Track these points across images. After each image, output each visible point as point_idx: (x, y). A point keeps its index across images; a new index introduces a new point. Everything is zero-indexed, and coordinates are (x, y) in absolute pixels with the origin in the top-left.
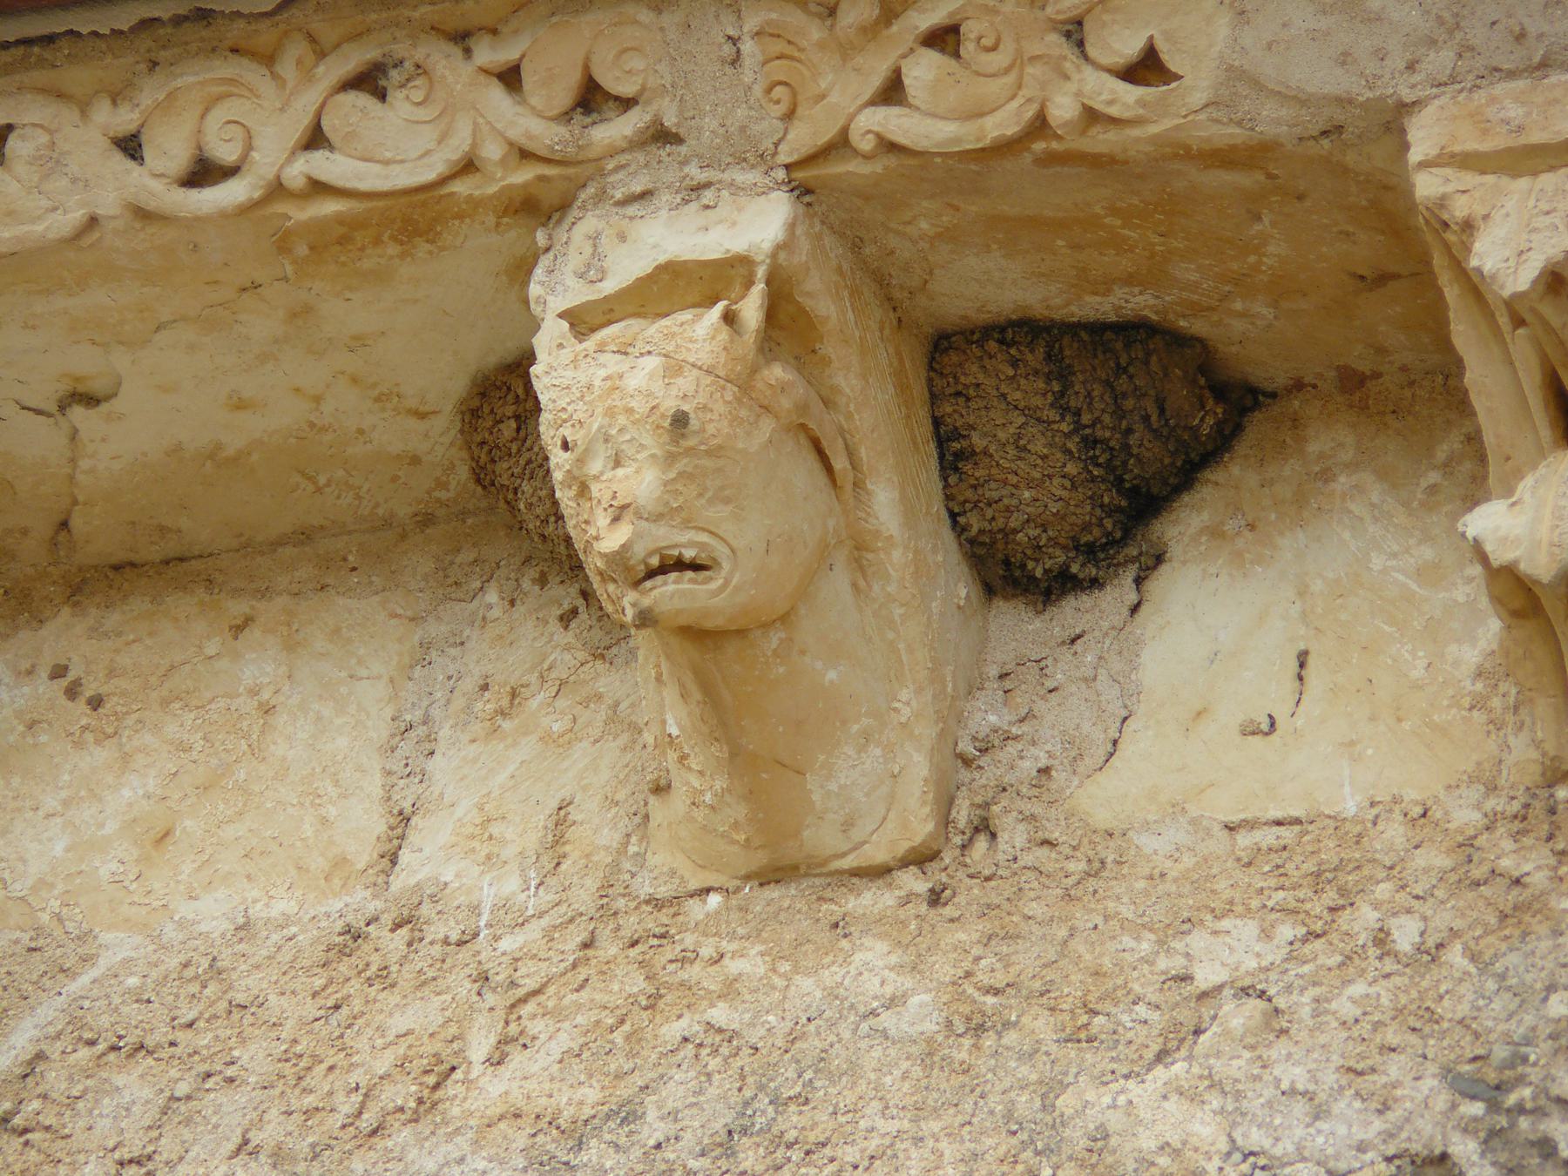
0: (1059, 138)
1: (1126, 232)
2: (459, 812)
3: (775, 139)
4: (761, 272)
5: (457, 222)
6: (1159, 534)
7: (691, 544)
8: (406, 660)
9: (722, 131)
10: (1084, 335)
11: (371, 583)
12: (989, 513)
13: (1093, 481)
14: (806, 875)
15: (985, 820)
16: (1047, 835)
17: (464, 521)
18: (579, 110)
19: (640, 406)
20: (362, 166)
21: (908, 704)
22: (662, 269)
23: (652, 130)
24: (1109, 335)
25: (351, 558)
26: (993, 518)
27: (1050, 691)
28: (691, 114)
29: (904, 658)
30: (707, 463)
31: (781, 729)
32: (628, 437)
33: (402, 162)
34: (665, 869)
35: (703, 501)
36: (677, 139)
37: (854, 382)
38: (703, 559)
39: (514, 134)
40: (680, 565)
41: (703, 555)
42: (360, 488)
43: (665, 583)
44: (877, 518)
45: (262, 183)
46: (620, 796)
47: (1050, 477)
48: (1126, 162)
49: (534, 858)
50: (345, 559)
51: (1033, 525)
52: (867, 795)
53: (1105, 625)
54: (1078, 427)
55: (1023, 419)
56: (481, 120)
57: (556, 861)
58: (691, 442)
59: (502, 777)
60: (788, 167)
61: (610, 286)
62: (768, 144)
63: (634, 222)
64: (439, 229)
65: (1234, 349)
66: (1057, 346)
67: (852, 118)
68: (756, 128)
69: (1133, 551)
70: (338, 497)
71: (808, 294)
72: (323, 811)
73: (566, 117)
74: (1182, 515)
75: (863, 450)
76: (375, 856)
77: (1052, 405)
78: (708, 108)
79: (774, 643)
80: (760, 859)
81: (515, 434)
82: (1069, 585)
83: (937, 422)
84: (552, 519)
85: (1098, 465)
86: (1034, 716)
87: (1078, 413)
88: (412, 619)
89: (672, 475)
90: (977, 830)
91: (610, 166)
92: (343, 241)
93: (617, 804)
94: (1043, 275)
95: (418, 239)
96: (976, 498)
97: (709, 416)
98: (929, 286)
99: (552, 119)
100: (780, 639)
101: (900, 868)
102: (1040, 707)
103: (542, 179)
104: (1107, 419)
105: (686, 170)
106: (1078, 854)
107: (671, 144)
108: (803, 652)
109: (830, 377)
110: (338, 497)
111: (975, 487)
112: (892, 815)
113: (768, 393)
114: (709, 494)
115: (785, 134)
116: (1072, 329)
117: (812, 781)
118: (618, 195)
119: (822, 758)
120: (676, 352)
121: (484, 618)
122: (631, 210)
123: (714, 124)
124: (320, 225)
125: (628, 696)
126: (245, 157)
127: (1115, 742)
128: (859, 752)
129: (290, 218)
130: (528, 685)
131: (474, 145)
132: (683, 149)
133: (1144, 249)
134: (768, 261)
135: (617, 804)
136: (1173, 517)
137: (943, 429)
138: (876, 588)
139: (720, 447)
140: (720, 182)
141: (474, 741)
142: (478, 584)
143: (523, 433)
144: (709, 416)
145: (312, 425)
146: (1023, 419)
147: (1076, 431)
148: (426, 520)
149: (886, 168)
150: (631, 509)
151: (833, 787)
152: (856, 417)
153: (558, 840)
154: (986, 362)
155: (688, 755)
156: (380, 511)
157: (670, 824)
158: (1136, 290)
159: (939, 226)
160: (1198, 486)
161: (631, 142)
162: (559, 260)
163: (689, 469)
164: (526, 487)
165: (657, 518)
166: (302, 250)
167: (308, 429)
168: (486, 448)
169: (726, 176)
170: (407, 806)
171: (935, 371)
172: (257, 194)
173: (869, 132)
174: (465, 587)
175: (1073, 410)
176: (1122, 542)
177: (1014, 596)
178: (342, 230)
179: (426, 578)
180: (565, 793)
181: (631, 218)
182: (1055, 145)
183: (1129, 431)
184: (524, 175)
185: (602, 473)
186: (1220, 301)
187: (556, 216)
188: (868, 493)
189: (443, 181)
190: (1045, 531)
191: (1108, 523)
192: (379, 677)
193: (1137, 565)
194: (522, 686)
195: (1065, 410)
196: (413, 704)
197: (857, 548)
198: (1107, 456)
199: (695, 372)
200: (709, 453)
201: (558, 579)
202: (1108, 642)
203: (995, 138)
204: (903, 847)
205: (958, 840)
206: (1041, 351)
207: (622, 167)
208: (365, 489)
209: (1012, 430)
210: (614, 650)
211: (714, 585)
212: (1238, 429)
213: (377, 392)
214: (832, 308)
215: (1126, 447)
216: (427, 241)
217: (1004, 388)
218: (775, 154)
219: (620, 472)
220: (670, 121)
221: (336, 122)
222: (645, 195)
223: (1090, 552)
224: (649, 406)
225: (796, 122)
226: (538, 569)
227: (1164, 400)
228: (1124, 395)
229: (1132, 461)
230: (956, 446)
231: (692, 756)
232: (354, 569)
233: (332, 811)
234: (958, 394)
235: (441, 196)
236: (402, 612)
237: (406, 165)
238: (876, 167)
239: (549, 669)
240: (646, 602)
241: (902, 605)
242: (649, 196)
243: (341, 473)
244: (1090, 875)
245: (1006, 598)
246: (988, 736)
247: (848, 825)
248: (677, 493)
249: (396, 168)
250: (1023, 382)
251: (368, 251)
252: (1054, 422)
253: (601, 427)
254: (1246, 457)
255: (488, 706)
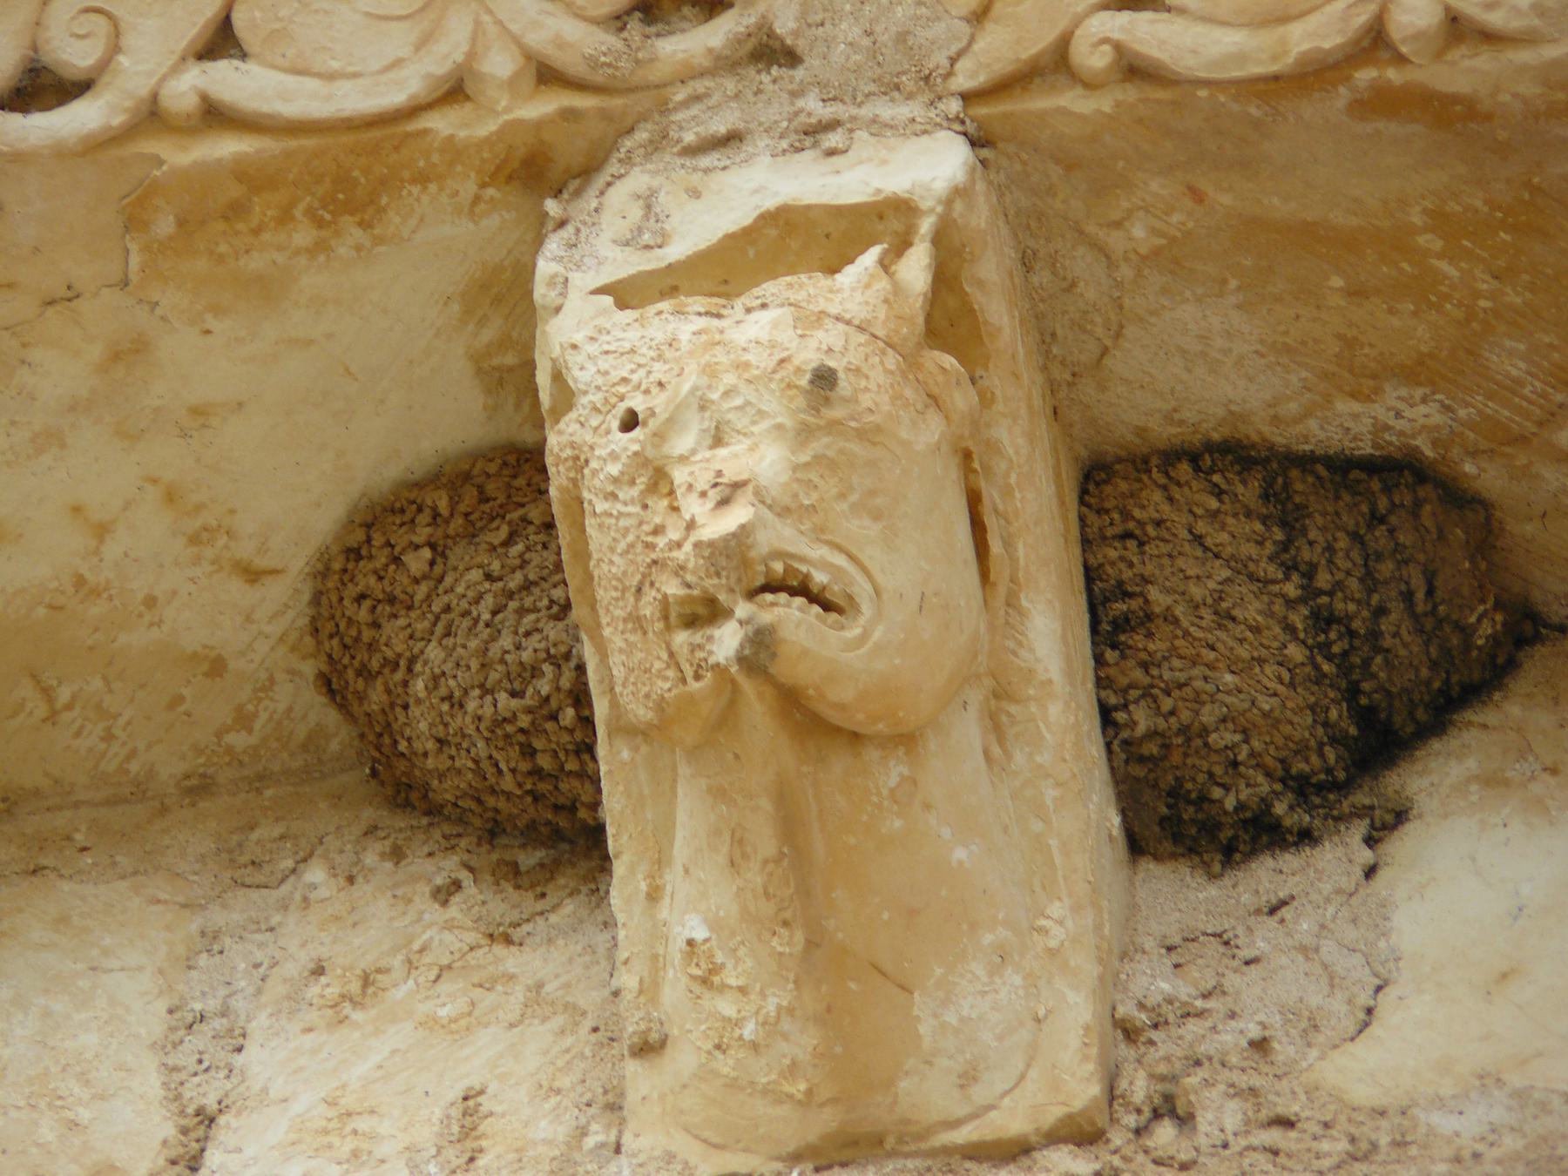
0: (1401, 60)
1: (1444, 266)
2: (297, 1108)
3: (954, 48)
4: (926, 226)
5: (416, 190)
6: (1397, 787)
7: (825, 565)
8: (181, 950)
9: (866, 42)
10: (1321, 470)
11: (114, 864)
12: (1167, 704)
13: (1317, 683)
14: (893, 1154)
15: (1168, 1098)
16: (1280, 1110)
17: (259, 791)
18: (638, 15)
19: (761, 360)
20: (291, 81)
21: (1061, 923)
22: (768, 218)
23: (750, 45)
24: (1355, 474)
25: (78, 837)
26: (1172, 713)
27: (1247, 963)
28: (818, 18)
29: (1058, 860)
30: (854, 447)
31: (886, 916)
32: (739, 401)
33: (355, 75)
34: (656, 1153)
35: (845, 506)
36: (791, 58)
37: (1020, 441)
38: (835, 594)
39: (537, 40)
40: (803, 590)
41: (836, 588)
42: (116, 716)
43: (788, 606)
44: (1032, 650)
45: (128, 104)
46: (565, 1082)
47: (1261, 661)
48: (1488, 117)
49: (433, 1151)
50: (69, 838)
51: (1231, 726)
52: (1000, 1038)
53: (1327, 888)
54: (1310, 592)
55: (1226, 573)
56: (486, 18)
57: (469, 1155)
58: (837, 413)
59: (364, 1068)
60: (967, 97)
61: (676, 251)
62: (940, 59)
63: (712, 175)
64: (384, 200)
65: (1529, 529)
66: (1280, 480)
67: (1078, 22)
68: (923, 35)
69: (1361, 798)
70: (78, 734)
71: (980, 283)
72: (70, 1115)
73: (618, 21)
74: (1433, 765)
75: (1020, 546)
76: (161, 1162)
77: (1271, 559)
78: (848, 7)
79: (893, 780)
80: (825, 1121)
81: (427, 568)
82: (1265, 839)
83: (1091, 575)
84: (477, 692)
85: (1329, 658)
86: (1224, 993)
87: (1310, 573)
88: (184, 906)
89: (805, 458)
90: (1157, 1115)
91: (679, 97)
92: (235, 211)
93: (558, 1092)
94: (1288, 350)
95: (348, 218)
96: (1147, 680)
97: (863, 383)
98: (1107, 361)
99: (596, 22)
100: (901, 775)
101: (1046, 1146)
102: (1232, 981)
103: (568, 115)
104: (1354, 584)
105: (800, 103)
106: (1334, 1132)
107: (780, 66)
108: (927, 807)
109: (988, 425)
110: (78, 734)
111: (1145, 666)
112: (1033, 1074)
113: (940, 378)
114: (854, 498)
115: (970, 44)
116: (1305, 462)
117: (921, 1005)
118: (689, 138)
119: (938, 971)
120: (809, 302)
121: (305, 899)
122: (706, 161)
123: (855, 32)
124: (205, 175)
125: (557, 976)
126: (104, 65)
127: (1369, 1011)
128: (991, 974)
129: (161, 162)
130: (387, 971)
131: (471, 55)
132: (799, 73)
133: (1460, 305)
134: (939, 209)
135: (558, 1092)
136: (1418, 767)
137: (1098, 586)
138: (1019, 758)
139: (878, 429)
140: (853, 119)
141: (310, 1030)
142: (290, 863)
143: (438, 569)
144: (863, 383)
145: (80, 581)
146: (1226, 573)
147: (1302, 600)
148: (198, 788)
149: (1118, 104)
150: (750, 487)
151: (951, 1018)
152: (1018, 495)
153: (467, 1132)
154: (1176, 492)
155: (723, 966)
156: (134, 767)
157: (662, 1097)
158: (1419, 393)
159: (1162, 234)
160: (1453, 731)
161: (718, 58)
162: (584, 231)
163: (831, 453)
164: (434, 652)
165: (784, 512)
166: (165, 226)
167: (70, 590)
168: (367, 604)
169: (866, 112)
170: (211, 1102)
171: (1089, 506)
172: (118, 120)
173: (1105, 41)
174: (267, 868)
175: (1303, 567)
176: (1343, 788)
177: (1173, 856)
178: (235, 191)
179: (202, 858)
180: (475, 1081)
181: (707, 171)
182: (1393, 75)
183: (1381, 611)
184: (543, 106)
185: (694, 452)
186: (1540, 424)
187: (574, 185)
188: (1022, 613)
189: (414, 110)
190: (1246, 741)
191: (1331, 755)
192: (140, 969)
193: (1367, 821)
194: (379, 971)
195: (1289, 569)
196: (204, 994)
197: (996, 696)
198: (1345, 644)
199: (841, 326)
200: (863, 435)
201: (426, 849)
202: (1331, 910)
203: (1305, 53)
204: (1052, 1115)
205: (1131, 1120)
206: (1255, 485)
207: (697, 98)
208: (122, 721)
209: (1212, 585)
210: (526, 928)
211: (854, 632)
212: (1512, 665)
213: (197, 523)
214: (1006, 319)
215: (1375, 635)
216: (360, 224)
217: (1201, 527)
218: (950, 74)
219: (722, 452)
220: (785, 25)
221: (257, 14)
222: (731, 139)
223: (1302, 788)
224: (777, 357)
225: (989, 26)
226: (387, 843)
227: (1434, 574)
228: (1379, 557)
229: (1379, 659)
230: (1120, 607)
231: (729, 966)
232: (85, 849)
233: (84, 1114)
234: (1128, 535)
235: (409, 135)
236: (167, 897)
237: (360, 81)
238: (1103, 103)
239: (421, 951)
240: (767, 617)
241: (1058, 784)
242: (736, 143)
243: (97, 683)
244: (1356, 1159)
245: (1158, 858)
246: (1159, 1005)
247: (968, 1078)
248: (809, 484)
249: (344, 86)
250: (1230, 520)
251: (266, 236)
252: (1274, 582)
253: (695, 389)
254: (1529, 696)
255: (328, 991)
